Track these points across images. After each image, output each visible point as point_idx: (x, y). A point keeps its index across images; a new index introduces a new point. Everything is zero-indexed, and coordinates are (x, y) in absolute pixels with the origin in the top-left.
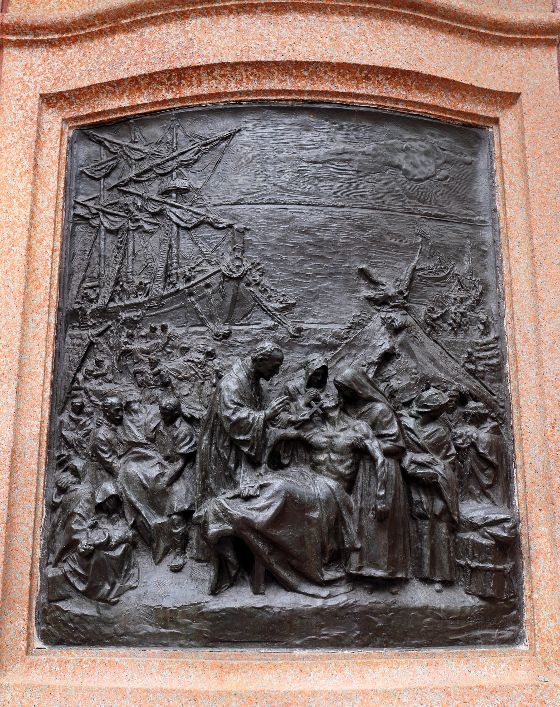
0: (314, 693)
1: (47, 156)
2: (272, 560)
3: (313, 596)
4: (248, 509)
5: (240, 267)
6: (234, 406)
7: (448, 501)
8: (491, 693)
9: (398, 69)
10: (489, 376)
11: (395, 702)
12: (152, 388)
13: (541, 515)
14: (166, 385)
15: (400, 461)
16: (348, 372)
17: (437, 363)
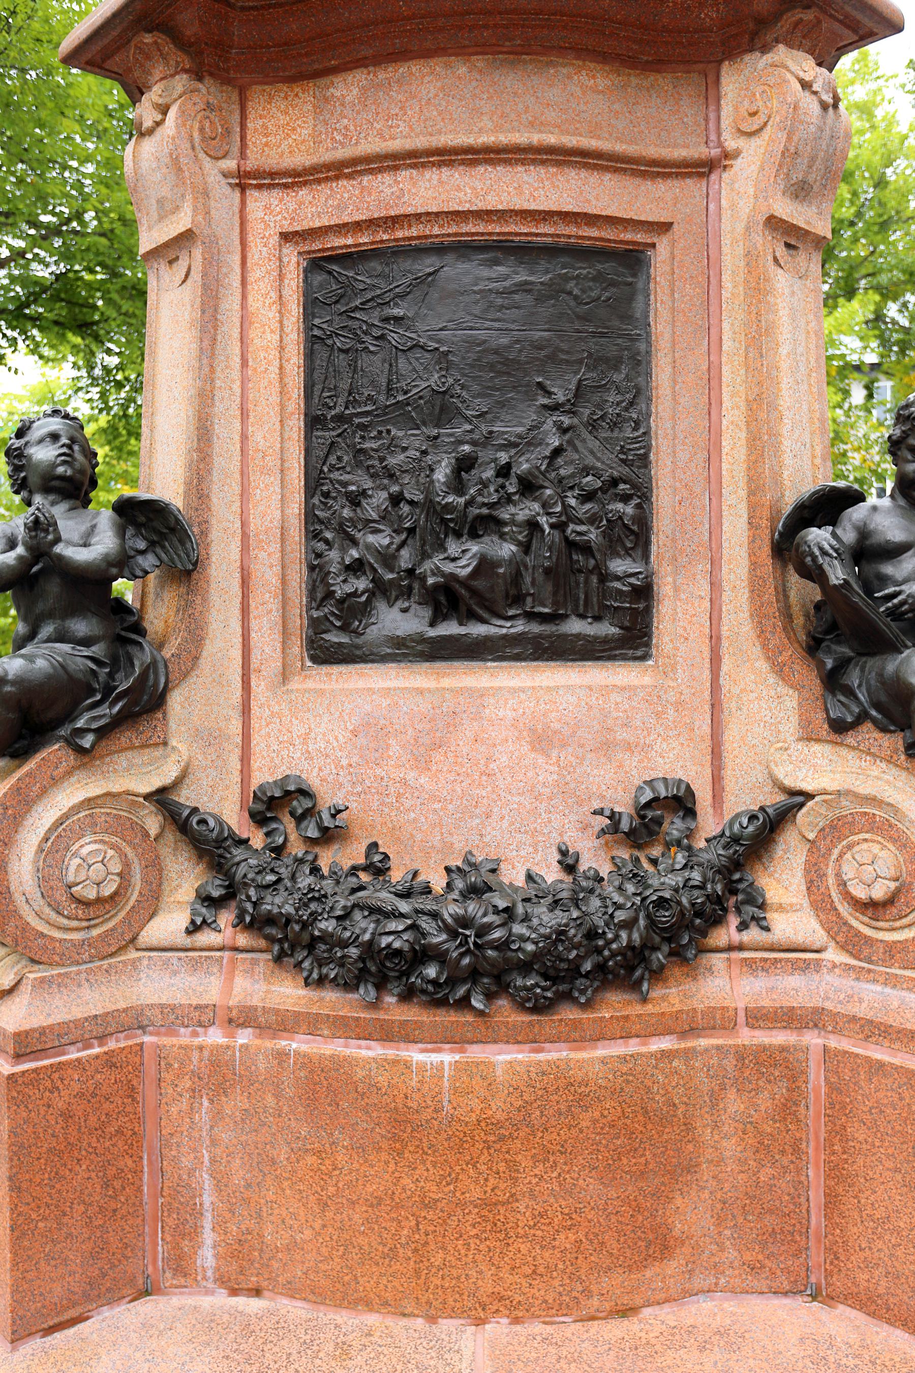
0: (500, 688)
2: (472, 602)
3: (500, 626)
14: (391, 476)
15: (564, 531)
16: (525, 466)
17: (598, 455)
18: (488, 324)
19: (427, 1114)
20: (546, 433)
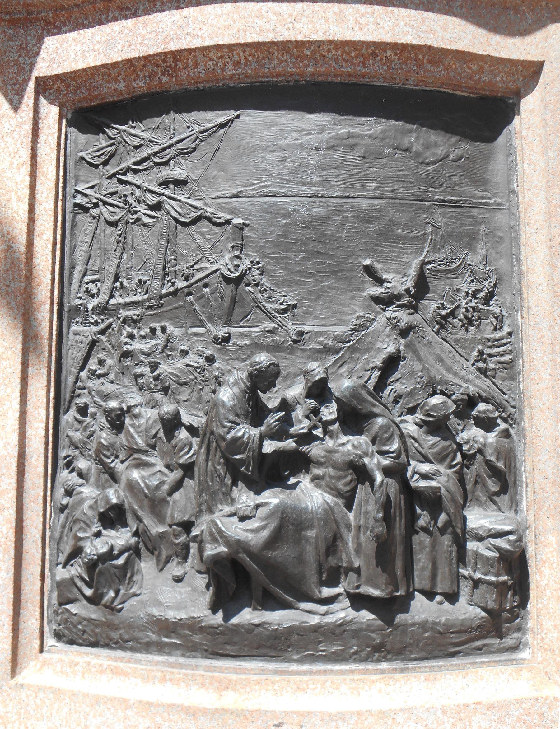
1: (45, 143)
4: (244, 530)
5: (239, 266)
6: (229, 424)
7: (451, 514)
8: (488, 709)
9: (407, 44)
10: (501, 374)
11: (390, 722)
12: (152, 392)
13: (549, 524)
14: (165, 390)
16: (347, 383)
18: (298, 189)
20: (377, 334)
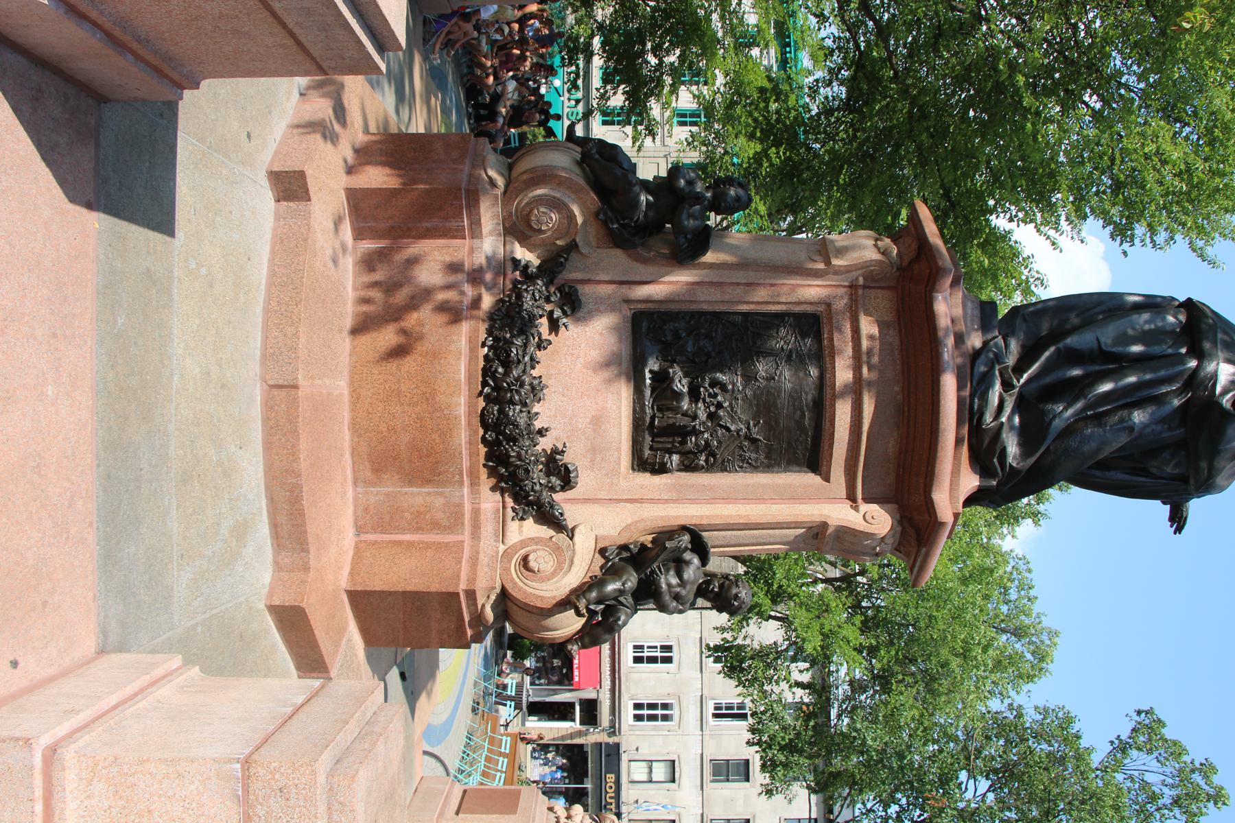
19: (438, 367)
